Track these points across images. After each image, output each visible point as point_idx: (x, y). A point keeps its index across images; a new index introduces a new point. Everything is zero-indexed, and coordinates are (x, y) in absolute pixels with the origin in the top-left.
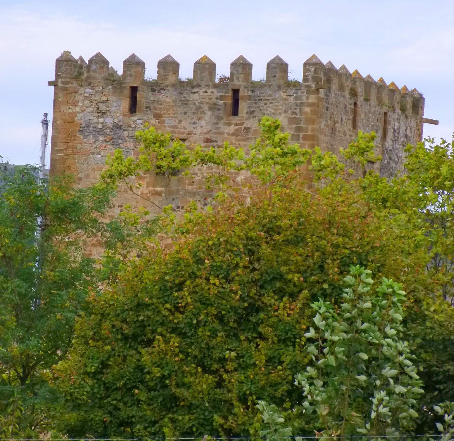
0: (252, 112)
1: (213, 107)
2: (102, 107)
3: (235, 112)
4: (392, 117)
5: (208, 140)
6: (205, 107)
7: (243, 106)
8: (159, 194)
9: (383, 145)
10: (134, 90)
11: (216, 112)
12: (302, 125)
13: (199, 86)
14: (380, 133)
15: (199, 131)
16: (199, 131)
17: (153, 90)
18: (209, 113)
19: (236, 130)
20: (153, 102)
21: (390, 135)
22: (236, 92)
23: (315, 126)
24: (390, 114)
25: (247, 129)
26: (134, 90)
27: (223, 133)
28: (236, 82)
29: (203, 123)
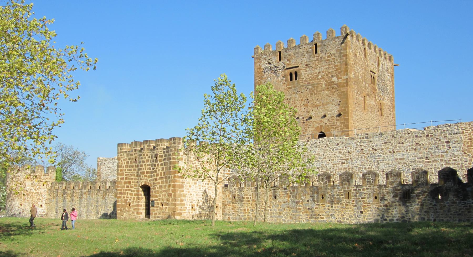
0: (322, 51)
1: (307, 52)
2: (270, 61)
3: (316, 52)
4: (382, 59)
5: (307, 65)
6: (305, 53)
7: (319, 49)
8: (291, 88)
9: (378, 68)
10: (280, 52)
11: (309, 54)
12: (342, 51)
13: (302, 46)
14: (377, 63)
15: (303, 62)
16: (303, 62)
17: (286, 51)
18: (307, 55)
19: (317, 59)
20: (286, 55)
21: (381, 65)
22: (316, 45)
23: (390, 229)
24: (380, 57)
25: (321, 58)
26: (280, 52)
27: (312, 61)
28: (316, 41)
29: (305, 59)
